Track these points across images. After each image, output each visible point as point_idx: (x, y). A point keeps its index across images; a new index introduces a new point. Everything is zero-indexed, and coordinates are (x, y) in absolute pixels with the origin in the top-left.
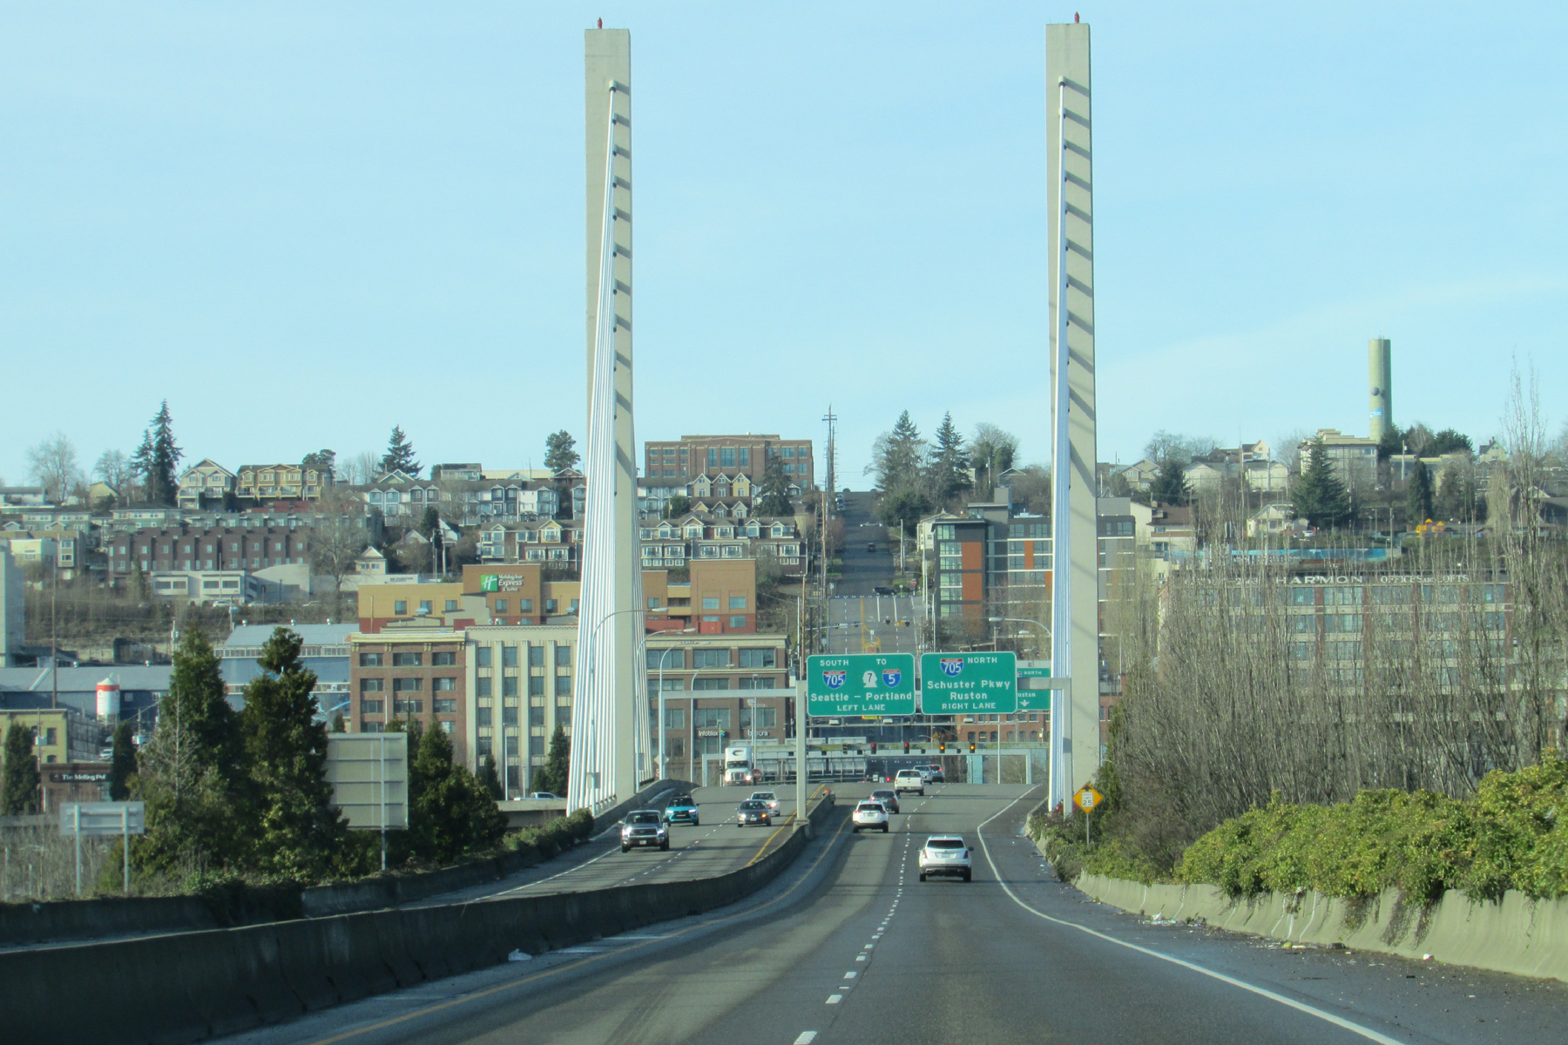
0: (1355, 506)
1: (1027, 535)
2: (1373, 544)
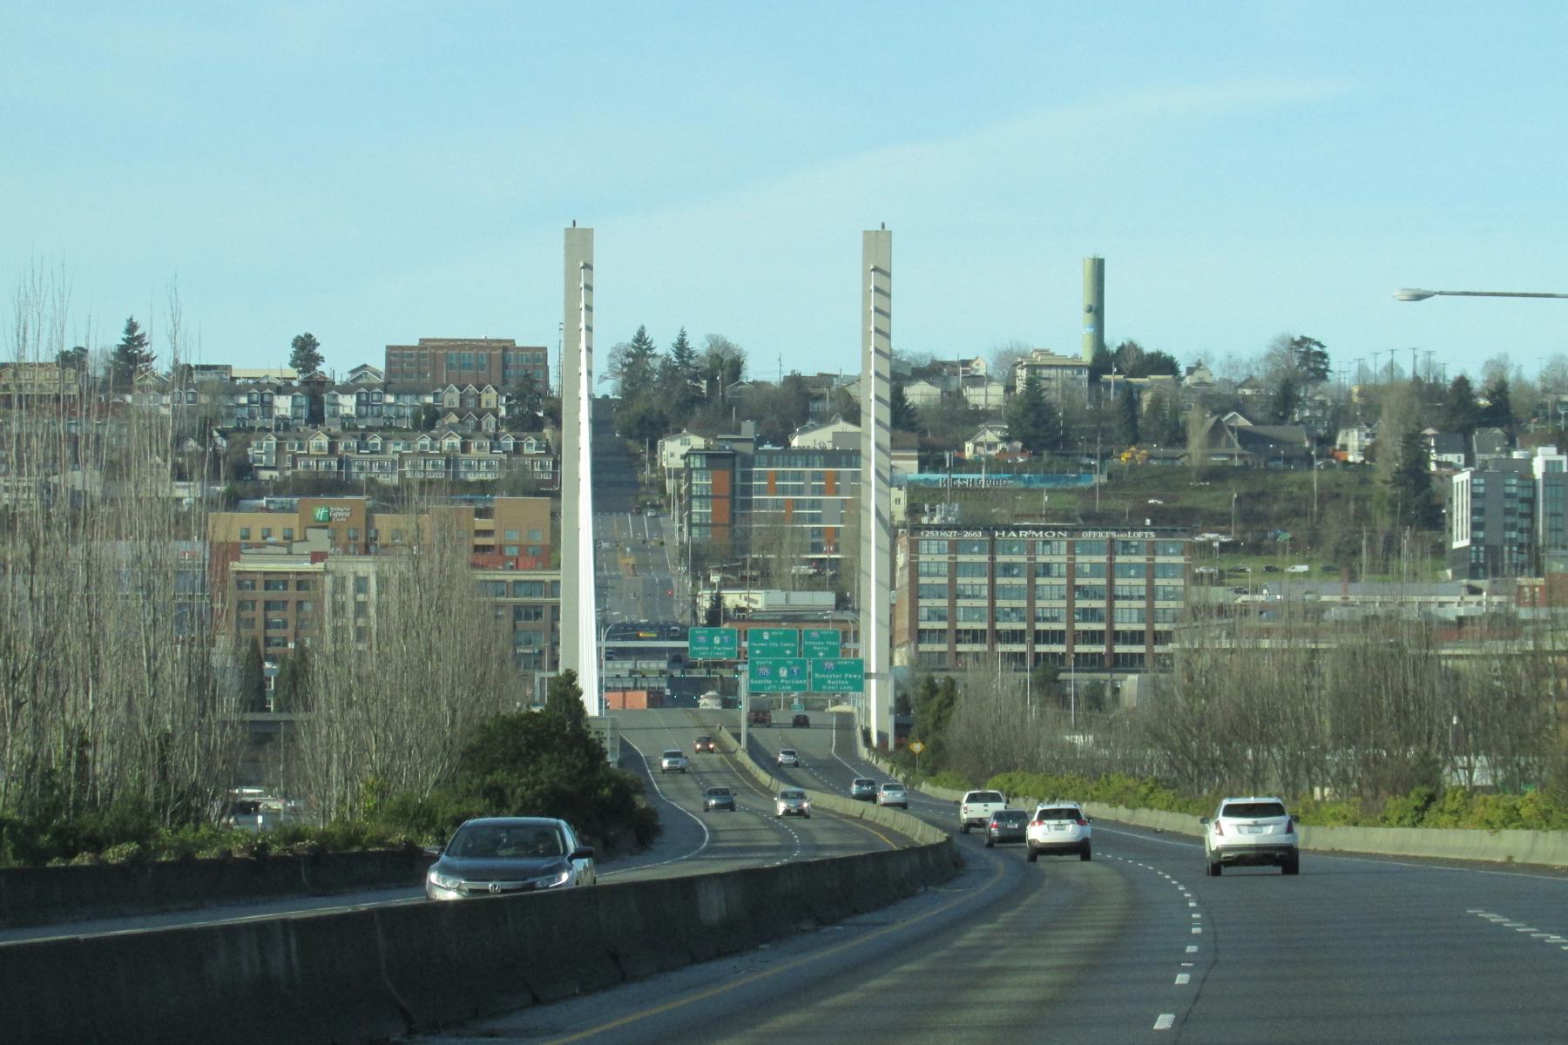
1: (770, 465)
2: (1081, 470)
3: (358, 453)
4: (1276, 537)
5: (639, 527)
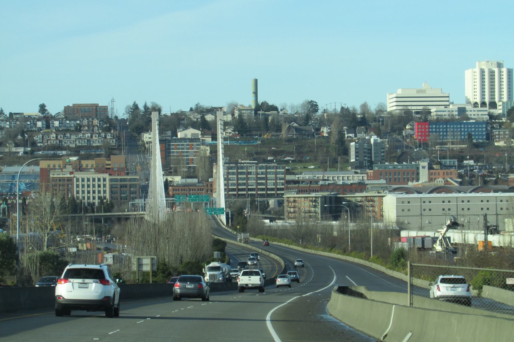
0: (249, 128)
2: (254, 140)
3: (64, 139)
4: (306, 158)
5: (140, 158)
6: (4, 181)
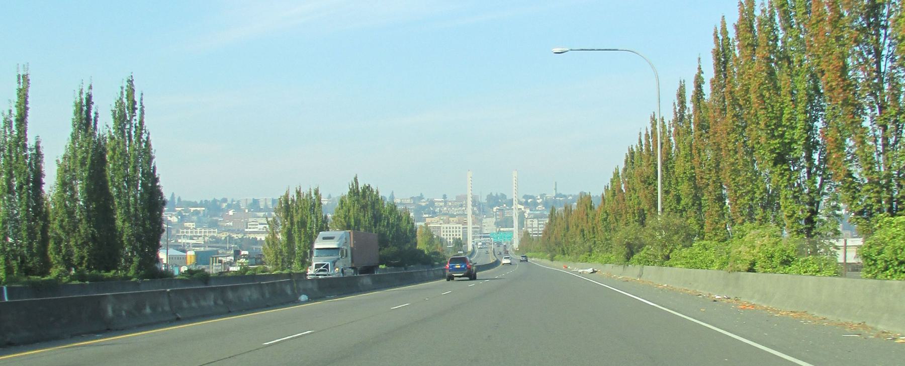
6: (902, 219)
